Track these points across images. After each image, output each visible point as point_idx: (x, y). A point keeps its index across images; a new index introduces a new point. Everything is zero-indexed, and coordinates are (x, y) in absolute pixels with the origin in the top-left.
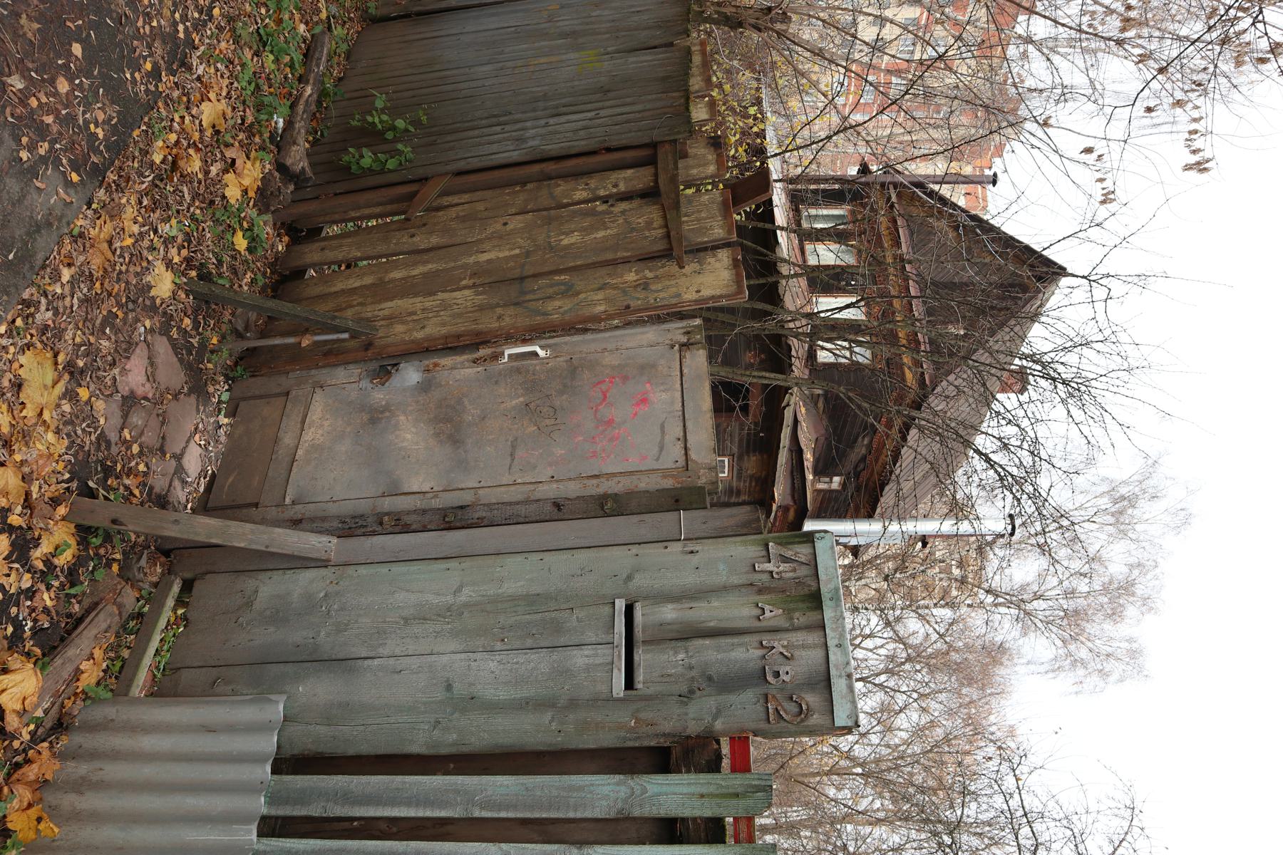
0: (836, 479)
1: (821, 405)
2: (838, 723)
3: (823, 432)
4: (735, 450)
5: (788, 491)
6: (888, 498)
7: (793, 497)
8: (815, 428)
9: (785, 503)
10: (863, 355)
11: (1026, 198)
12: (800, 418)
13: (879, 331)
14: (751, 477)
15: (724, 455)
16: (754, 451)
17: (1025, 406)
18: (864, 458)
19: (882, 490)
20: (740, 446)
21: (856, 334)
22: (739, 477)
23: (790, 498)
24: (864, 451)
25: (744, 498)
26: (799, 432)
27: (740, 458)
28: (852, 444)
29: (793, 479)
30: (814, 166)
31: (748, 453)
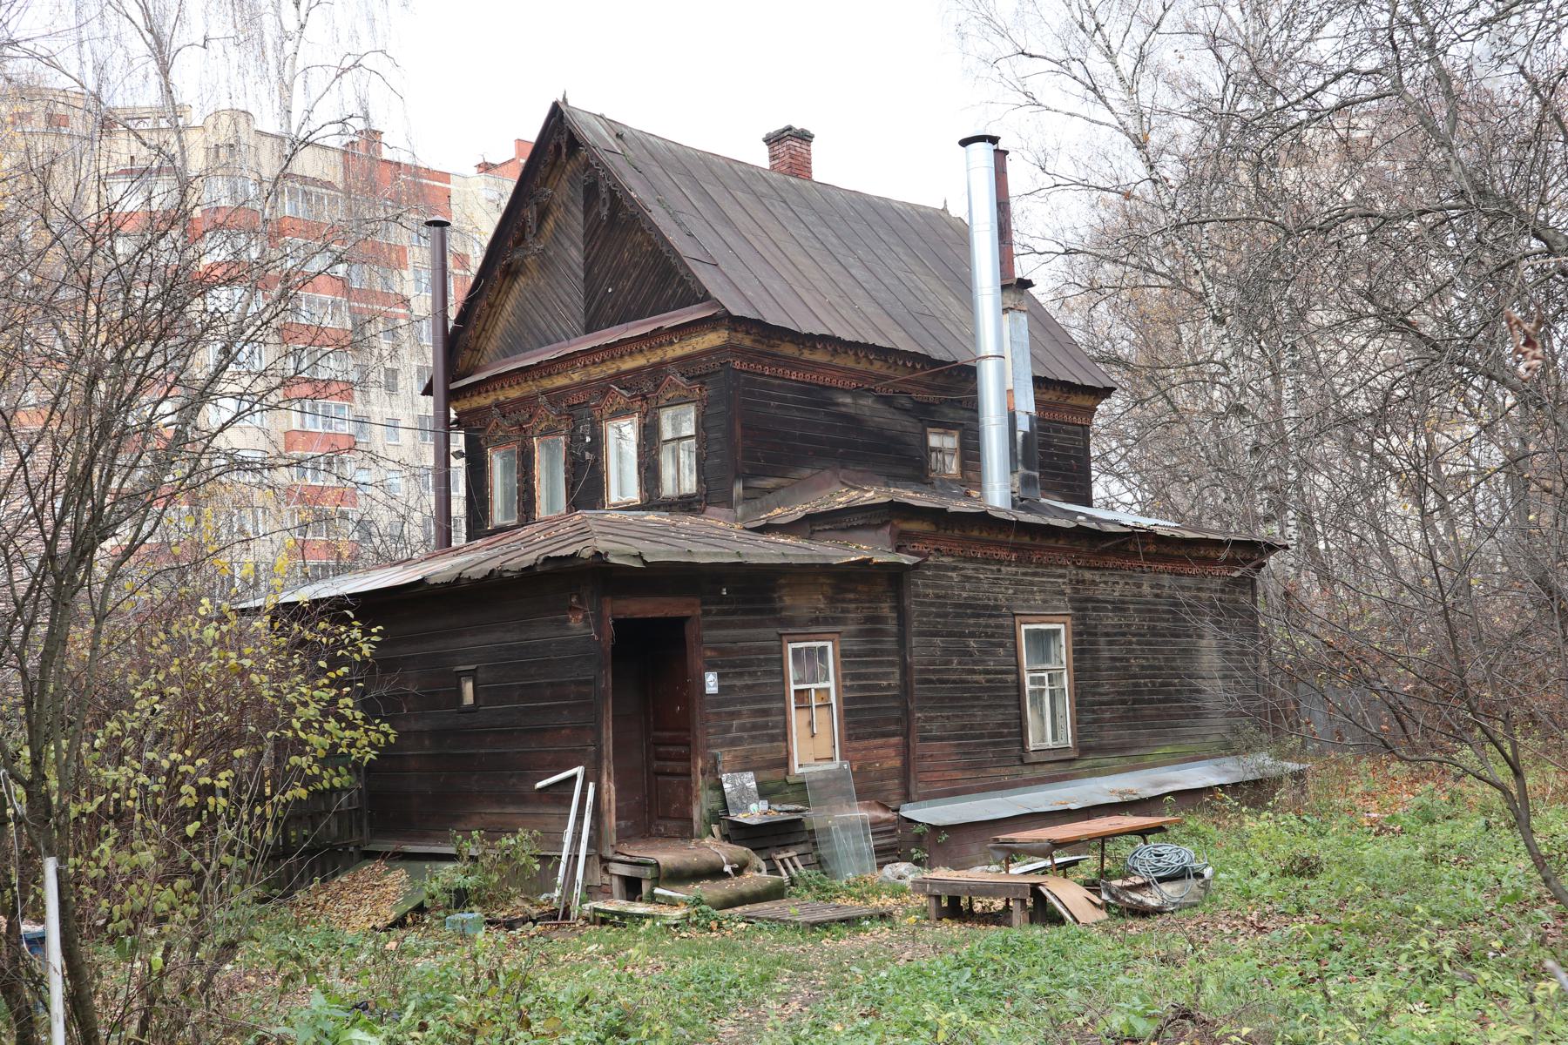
0: (934, 441)
1: (769, 483)
2: (668, 489)
4: (772, 632)
5: (871, 535)
6: (963, 359)
8: (819, 488)
9: (888, 538)
11: (471, 148)
13: (645, 394)
14: (832, 600)
15: (781, 650)
16: (771, 600)
18: (887, 400)
22: (835, 621)
23: (881, 532)
25: (886, 609)
27: (789, 622)
28: (853, 422)
29: (853, 528)
31: (774, 611)
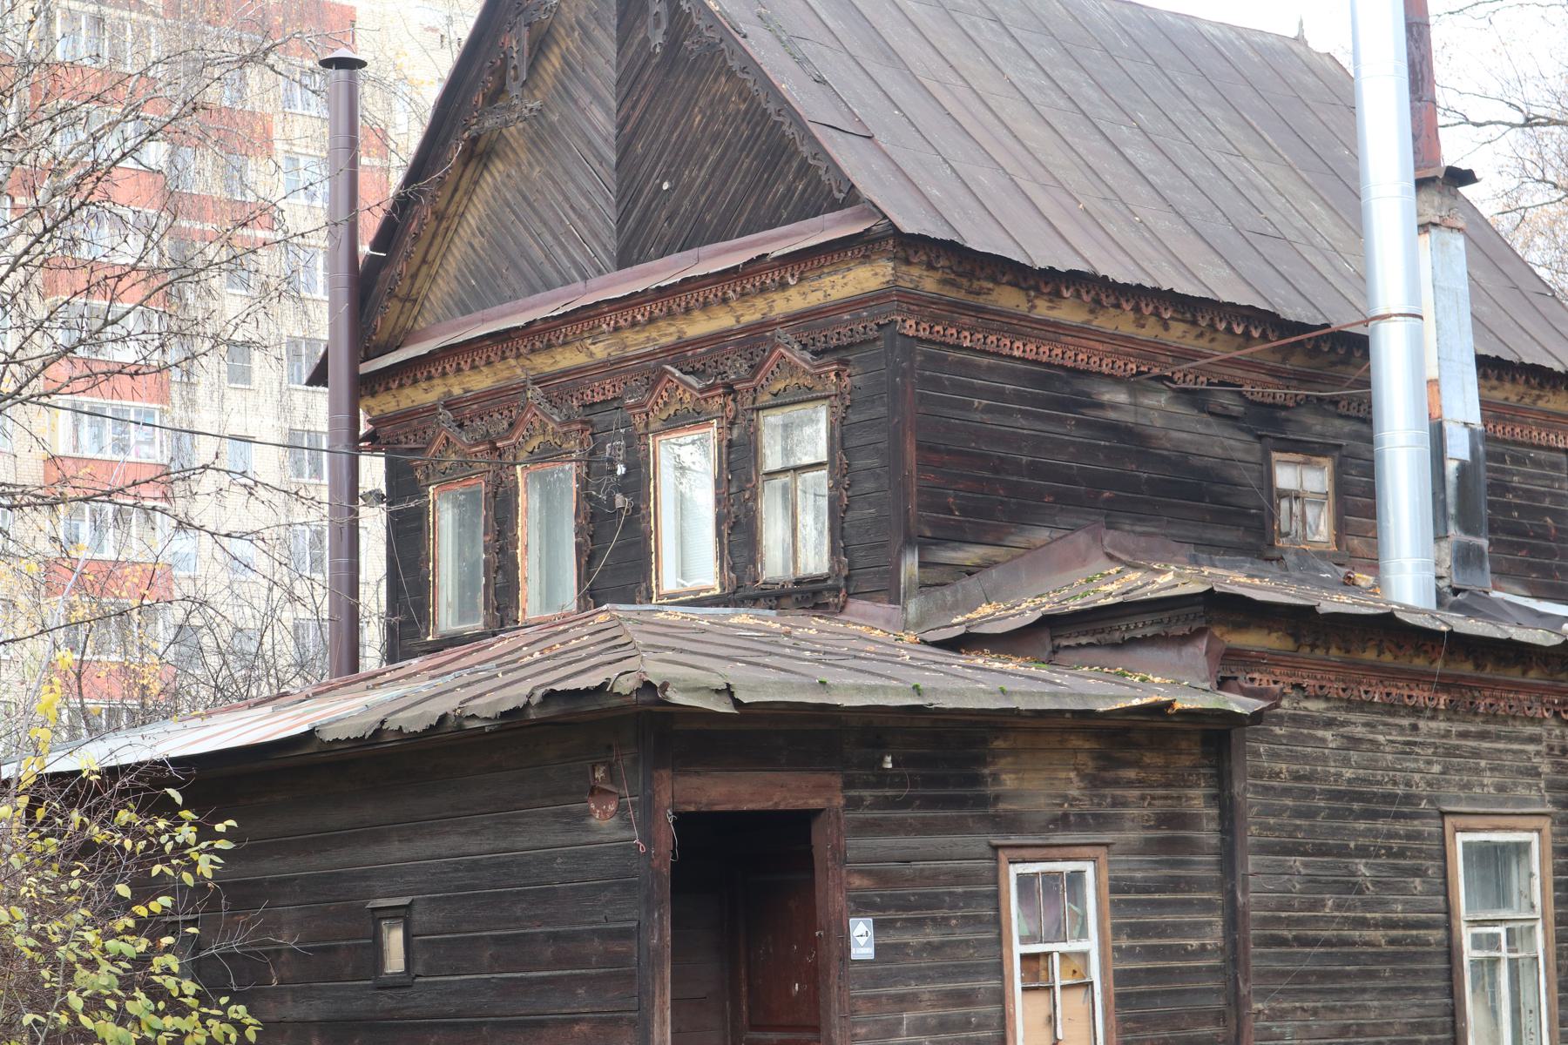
0: (1286, 476)
1: (970, 555)
3: (1081, 538)
4: (977, 842)
5: (1168, 655)
7: (1185, 640)
9: (1202, 662)
10: (801, 437)
12: (1027, 610)
13: (732, 383)
14: (1094, 782)
17: (239, 251)
19: (1301, 327)
20: (957, 827)
21: (1026, 372)
22: (1101, 822)
23: (1189, 651)
24: (1159, 400)
25: (1197, 800)
26: (998, 628)
27: (1011, 824)
28: (1130, 437)
29: (1134, 642)
30: (256, 602)
31: (982, 801)
